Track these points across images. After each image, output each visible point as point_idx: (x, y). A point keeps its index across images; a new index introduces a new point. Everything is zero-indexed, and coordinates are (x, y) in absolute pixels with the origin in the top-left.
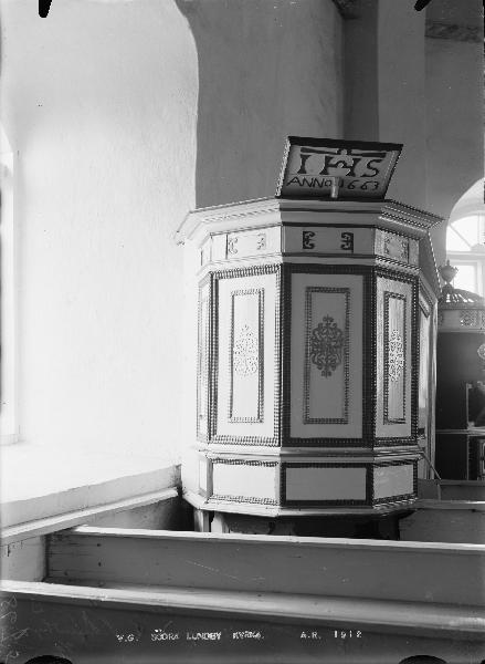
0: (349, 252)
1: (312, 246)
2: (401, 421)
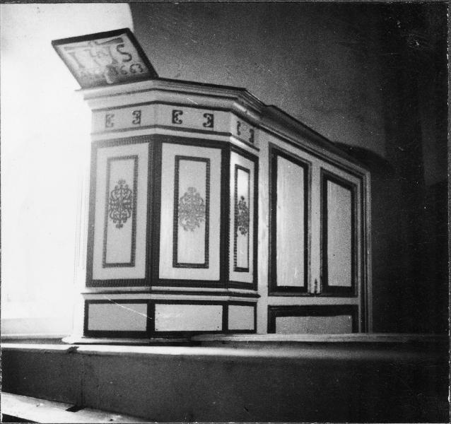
0: (138, 125)
2: (246, 270)
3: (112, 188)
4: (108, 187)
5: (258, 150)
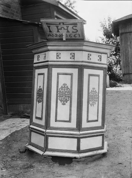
0: (73, 60)
1: (60, 58)
4: (58, 86)
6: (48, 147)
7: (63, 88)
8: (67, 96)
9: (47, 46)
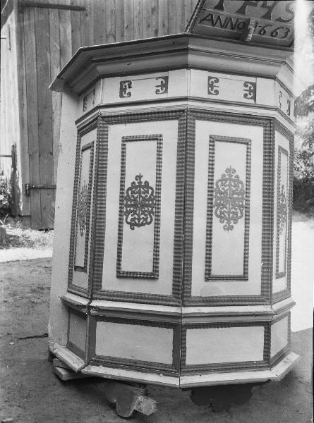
0: (252, 101)
1: (217, 92)
3: (128, 185)
4: (122, 186)
5: (14, 147)
6: (185, 360)
7: (226, 180)
8: (146, 211)
9: (186, 51)
